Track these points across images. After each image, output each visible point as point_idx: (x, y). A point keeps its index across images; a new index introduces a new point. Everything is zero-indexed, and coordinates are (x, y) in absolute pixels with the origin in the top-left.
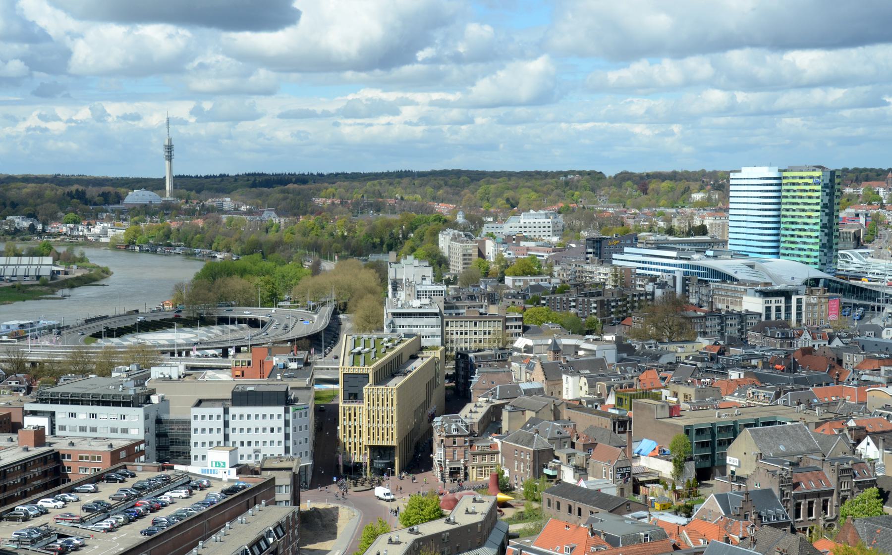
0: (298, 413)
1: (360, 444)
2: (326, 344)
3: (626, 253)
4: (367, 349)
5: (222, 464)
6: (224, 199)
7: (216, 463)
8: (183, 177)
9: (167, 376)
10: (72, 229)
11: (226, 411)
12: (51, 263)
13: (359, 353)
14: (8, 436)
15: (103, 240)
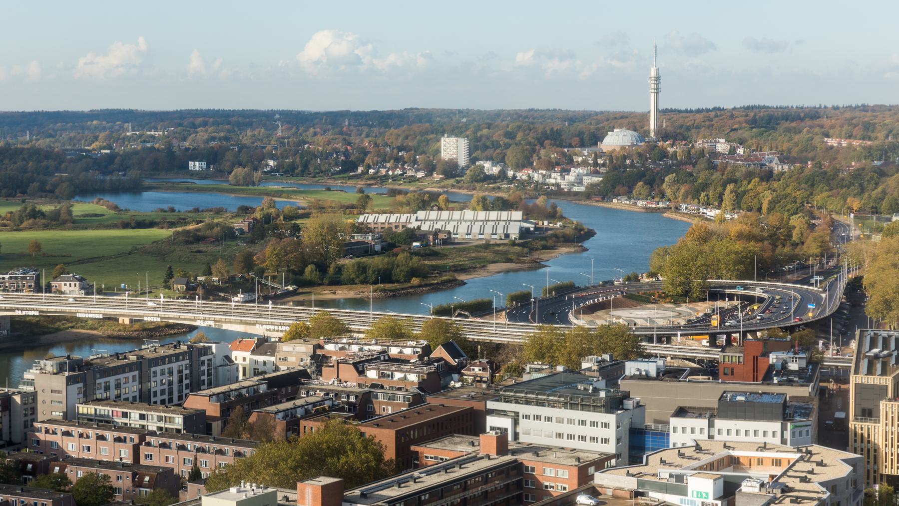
0: (797, 431)
1: (875, 472)
2: (837, 332)
3: (814, 454)
4: (885, 352)
5: (704, 495)
6: (717, 140)
7: (698, 492)
8: (671, 111)
9: (643, 373)
10: (544, 176)
11: (711, 425)
12: (521, 219)
13: (876, 357)
14: (470, 438)
15: (576, 189)
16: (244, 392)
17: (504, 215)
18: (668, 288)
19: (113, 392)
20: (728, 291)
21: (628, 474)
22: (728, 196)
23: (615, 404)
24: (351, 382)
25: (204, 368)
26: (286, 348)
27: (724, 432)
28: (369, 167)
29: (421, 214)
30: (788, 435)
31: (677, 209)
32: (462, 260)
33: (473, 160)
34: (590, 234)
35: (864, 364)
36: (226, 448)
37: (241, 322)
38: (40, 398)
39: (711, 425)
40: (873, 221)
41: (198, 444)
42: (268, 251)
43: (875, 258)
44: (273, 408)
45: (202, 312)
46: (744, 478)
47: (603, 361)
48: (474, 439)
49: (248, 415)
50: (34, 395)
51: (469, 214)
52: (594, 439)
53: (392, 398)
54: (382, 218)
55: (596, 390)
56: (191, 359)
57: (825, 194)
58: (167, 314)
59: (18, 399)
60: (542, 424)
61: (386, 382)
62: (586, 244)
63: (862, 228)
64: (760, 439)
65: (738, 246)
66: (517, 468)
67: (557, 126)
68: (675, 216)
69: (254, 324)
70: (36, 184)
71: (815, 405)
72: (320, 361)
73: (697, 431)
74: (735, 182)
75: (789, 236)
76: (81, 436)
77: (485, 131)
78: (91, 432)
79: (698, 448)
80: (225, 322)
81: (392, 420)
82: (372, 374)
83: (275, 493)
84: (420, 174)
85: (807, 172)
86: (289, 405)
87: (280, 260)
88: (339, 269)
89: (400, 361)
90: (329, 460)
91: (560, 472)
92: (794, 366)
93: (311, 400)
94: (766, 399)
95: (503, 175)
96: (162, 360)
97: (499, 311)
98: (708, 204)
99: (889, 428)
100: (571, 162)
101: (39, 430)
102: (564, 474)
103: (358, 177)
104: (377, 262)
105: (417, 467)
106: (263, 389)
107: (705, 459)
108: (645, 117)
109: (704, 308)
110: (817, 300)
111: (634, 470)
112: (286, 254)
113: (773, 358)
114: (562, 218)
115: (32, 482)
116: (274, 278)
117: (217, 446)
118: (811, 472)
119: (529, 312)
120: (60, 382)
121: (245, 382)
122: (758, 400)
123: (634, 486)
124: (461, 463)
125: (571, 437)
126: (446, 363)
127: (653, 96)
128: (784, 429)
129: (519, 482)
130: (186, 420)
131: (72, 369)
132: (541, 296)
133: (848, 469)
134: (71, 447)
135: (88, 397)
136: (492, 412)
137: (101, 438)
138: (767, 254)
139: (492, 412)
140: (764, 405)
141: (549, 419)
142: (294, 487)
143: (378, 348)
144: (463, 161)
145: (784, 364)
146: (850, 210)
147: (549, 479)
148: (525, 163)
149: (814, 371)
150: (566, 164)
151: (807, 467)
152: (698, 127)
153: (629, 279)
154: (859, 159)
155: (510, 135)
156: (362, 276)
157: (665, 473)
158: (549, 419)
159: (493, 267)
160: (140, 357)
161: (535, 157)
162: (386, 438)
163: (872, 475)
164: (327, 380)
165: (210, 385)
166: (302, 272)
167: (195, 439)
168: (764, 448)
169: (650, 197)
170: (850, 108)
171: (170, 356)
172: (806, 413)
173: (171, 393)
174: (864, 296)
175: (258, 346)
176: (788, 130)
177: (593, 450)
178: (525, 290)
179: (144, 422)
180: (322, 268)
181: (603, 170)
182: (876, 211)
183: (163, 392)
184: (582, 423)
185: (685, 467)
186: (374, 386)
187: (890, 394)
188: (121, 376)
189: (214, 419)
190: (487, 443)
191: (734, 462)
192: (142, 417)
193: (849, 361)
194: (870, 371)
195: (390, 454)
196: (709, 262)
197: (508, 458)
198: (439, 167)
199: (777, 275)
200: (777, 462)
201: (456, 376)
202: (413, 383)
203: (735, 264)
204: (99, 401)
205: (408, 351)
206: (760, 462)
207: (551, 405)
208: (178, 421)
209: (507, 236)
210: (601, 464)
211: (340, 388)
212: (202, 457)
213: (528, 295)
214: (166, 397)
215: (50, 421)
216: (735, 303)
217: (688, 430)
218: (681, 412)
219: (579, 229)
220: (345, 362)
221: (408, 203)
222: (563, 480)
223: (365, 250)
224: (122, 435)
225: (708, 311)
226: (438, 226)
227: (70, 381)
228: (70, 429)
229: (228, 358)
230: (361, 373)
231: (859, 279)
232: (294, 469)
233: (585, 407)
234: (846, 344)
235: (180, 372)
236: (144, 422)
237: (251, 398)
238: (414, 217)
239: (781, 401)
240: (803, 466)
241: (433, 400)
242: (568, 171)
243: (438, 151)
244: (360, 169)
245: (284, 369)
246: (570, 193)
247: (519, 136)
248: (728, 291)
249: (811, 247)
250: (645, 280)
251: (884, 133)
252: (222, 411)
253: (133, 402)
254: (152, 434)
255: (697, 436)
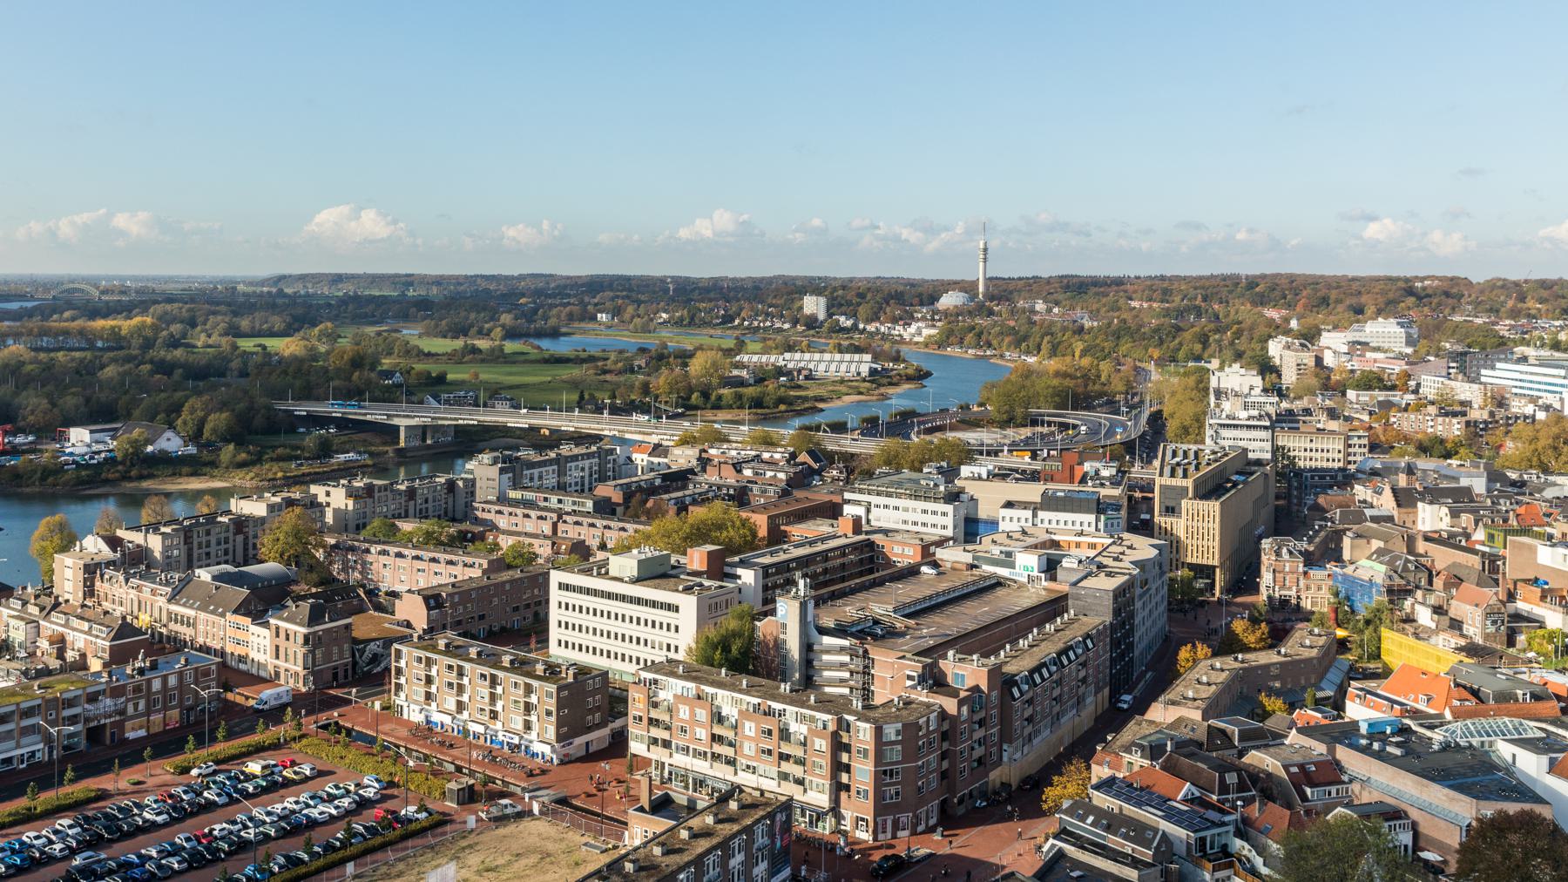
0: (1109, 522)
8: (996, 278)
11: (1035, 516)
13: (1178, 464)
15: (917, 339)
16: (642, 484)
17: (857, 357)
18: (995, 416)
19: (537, 483)
20: (1046, 418)
21: (965, 550)
22: (1045, 346)
23: (953, 497)
24: (731, 479)
25: (610, 466)
26: (677, 451)
27: (1046, 522)
28: (744, 320)
29: (788, 355)
30: (1101, 525)
31: (1002, 356)
32: (822, 392)
33: (830, 315)
34: (928, 374)
35: (1167, 470)
36: (627, 526)
37: (640, 433)
38: (478, 485)
39: (1035, 516)
40: (1172, 367)
41: (605, 523)
42: (661, 380)
43: (1173, 394)
44: (666, 496)
45: (607, 424)
46: (1064, 556)
47: (942, 467)
48: (834, 522)
49: (647, 501)
50: (473, 481)
51: (827, 356)
52: (934, 526)
53: (765, 491)
54: (755, 358)
55: (936, 485)
56: (599, 457)
57: (1129, 345)
58: (580, 425)
59: (460, 483)
60: (891, 512)
61: (758, 479)
62: (925, 382)
63: (1161, 374)
64: (1078, 527)
65: (1056, 382)
66: (870, 545)
67: (901, 288)
68: (1000, 362)
69: (650, 434)
70: (475, 329)
71: (1125, 502)
72: (704, 462)
73: (1023, 520)
74: (1052, 334)
75: (1099, 377)
76: (510, 514)
77: (840, 292)
78: (519, 511)
79: (1024, 532)
80: (628, 432)
81: (765, 508)
82: (748, 473)
83: (668, 556)
84: (786, 326)
85: (1113, 327)
86: (680, 494)
87: (671, 388)
88: (720, 398)
89: (772, 463)
90: (714, 534)
91: (906, 549)
92: (1105, 473)
93: (697, 491)
94: (1082, 496)
95: (855, 327)
96: (575, 458)
97: (853, 430)
98: (1028, 353)
99: (1190, 523)
100: (912, 318)
101: (477, 509)
102: (909, 551)
103: (735, 328)
104: (750, 391)
105: (785, 542)
106: (658, 482)
107: (1030, 541)
108: (975, 284)
109: (1026, 432)
110: (1125, 427)
111: (969, 547)
112: (677, 383)
113: (1088, 466)
114: (904, 361)
115: (471, 547)
116: (666, 402)
117: (621, 525)
118: (1123, 553)
119: (877, 431)
120: (494, 472)
121: (642, 477)
122: (1076, 495)
123: (970, 561)
124: (823, 540)
125: (915, 523)
126: (810, 466)
127: (981, 264)
128: (1097, 520)
129: (872, 557)
130: (595, 504)
131: (504, 462)
132: (887, 419)
133: (1156, 552)
134: (502, 522)
135: (515, 487)
136: (849, 502)
137: (527, 516)
138: (1080, 390)
139: (849, 502)
140: (1081, 500)
141: (897, 508)
142: (685, 554)
143: (754, 453)
144: (821, 316)
145: (1097, 472)
146: (1151, 357)
147: (896, 555)
148: (874, 317)
149: (1122, 477)
150: (908, 319)
151: (1120, 549)
152: (1019, 291)
153: (962, 408)
154: (1158, 317)
155: (862, 296)
156: (738, 401)
157: (996, 550)
158: (897, 508)
159: (847, 399)
160: (558, 454)
161: (882, 313)
162: (761, 522)
163: (1174, 563)
164: (711, 477)
165: (614, 479)
166: (689, 398)
167: (603, 519)
168: (1081, 534)
169: (978, 346)
170: (1150, 277)
171: (582, 455)
172: (1118, 508)
173: (583, 485)
174: (1164, 425)
175: (654, 449)
176: (1097, 294)
177: (934, 533)
178: (874, 414)
179: (561, 506)
180: (705, 395)
181: (939, 324)
182: (1174, 360)
183: (576, 484)
184: (925, 512)
185: (1014, 547)
186: (749, 482)
187: (1190, 495)
188: (543, 469)
189: (619, 505)
190: (844, 526)
191: (1056, 544)
192: (560, 501)
193: (1154, 474)
194: (1173, 475)
195: (763, 532)
196: (1030, 394)
197: (863, 537)
198: (802, 321)
199: (1089, 408)
200: (1093, 546)
201: (817, 477)
202: (781, 480)
203: (1052, 397)
204: (525, 488)
205: (777, 456)
206: (1078, 545)
207: (899, 496)
208: (589, 505)
209: (859, 374)
210: (941, 543)
211: (721, 482)
212: (608, 533)
213: (878, 418)
214: (579, 488)
215: (485, 502)
216: (1053, 429)
217: (1015, 520)
218: (1009, 505)
219: (919, 370)
220: (726, 463)
221: (776, 348)
222: (908, 557)
223: (741, 383)
224: (544, 514)
225: (1029, 434)
226: (802, 365)
227: (502, 471)
228: (502, 508)
229: (629, 458)
230: (739, 471)
231: (1160, 412)
232: (685, 539)
233: (926, 499)
234: (1149, 462)
235: (591, 468)
236: (561, 506)
237: (648, 489)
238: (781, 358)
239: (1095, 497)
240: (1114, 549)
241: (798, 494)
242: (910, 325)
243: (801, 308)
244: (737, 322)
245: (675, 468)
246: (910, 343)
247: (869, 296)
248: (1046, 418)
249: (1118, 385)
250: (976, 409)
251: (1180, 297)
252: (624, 499)
253: (552, 490)
254: (568, 513)
255: (1023, 523)
